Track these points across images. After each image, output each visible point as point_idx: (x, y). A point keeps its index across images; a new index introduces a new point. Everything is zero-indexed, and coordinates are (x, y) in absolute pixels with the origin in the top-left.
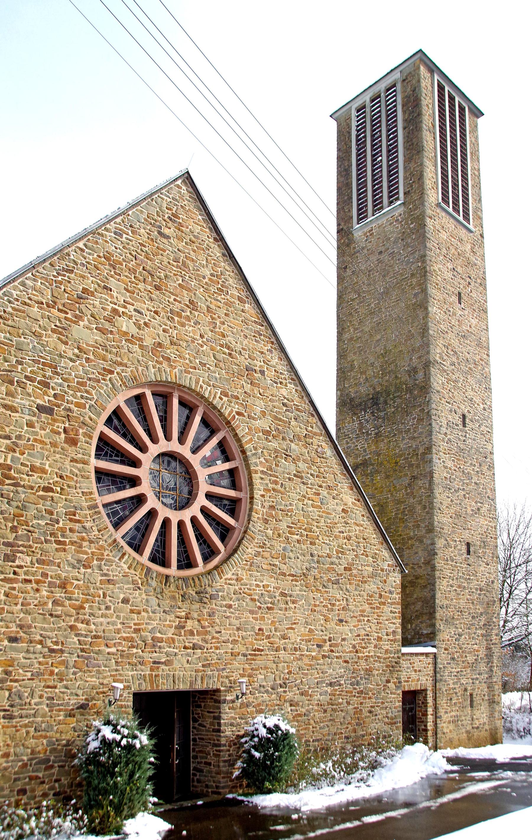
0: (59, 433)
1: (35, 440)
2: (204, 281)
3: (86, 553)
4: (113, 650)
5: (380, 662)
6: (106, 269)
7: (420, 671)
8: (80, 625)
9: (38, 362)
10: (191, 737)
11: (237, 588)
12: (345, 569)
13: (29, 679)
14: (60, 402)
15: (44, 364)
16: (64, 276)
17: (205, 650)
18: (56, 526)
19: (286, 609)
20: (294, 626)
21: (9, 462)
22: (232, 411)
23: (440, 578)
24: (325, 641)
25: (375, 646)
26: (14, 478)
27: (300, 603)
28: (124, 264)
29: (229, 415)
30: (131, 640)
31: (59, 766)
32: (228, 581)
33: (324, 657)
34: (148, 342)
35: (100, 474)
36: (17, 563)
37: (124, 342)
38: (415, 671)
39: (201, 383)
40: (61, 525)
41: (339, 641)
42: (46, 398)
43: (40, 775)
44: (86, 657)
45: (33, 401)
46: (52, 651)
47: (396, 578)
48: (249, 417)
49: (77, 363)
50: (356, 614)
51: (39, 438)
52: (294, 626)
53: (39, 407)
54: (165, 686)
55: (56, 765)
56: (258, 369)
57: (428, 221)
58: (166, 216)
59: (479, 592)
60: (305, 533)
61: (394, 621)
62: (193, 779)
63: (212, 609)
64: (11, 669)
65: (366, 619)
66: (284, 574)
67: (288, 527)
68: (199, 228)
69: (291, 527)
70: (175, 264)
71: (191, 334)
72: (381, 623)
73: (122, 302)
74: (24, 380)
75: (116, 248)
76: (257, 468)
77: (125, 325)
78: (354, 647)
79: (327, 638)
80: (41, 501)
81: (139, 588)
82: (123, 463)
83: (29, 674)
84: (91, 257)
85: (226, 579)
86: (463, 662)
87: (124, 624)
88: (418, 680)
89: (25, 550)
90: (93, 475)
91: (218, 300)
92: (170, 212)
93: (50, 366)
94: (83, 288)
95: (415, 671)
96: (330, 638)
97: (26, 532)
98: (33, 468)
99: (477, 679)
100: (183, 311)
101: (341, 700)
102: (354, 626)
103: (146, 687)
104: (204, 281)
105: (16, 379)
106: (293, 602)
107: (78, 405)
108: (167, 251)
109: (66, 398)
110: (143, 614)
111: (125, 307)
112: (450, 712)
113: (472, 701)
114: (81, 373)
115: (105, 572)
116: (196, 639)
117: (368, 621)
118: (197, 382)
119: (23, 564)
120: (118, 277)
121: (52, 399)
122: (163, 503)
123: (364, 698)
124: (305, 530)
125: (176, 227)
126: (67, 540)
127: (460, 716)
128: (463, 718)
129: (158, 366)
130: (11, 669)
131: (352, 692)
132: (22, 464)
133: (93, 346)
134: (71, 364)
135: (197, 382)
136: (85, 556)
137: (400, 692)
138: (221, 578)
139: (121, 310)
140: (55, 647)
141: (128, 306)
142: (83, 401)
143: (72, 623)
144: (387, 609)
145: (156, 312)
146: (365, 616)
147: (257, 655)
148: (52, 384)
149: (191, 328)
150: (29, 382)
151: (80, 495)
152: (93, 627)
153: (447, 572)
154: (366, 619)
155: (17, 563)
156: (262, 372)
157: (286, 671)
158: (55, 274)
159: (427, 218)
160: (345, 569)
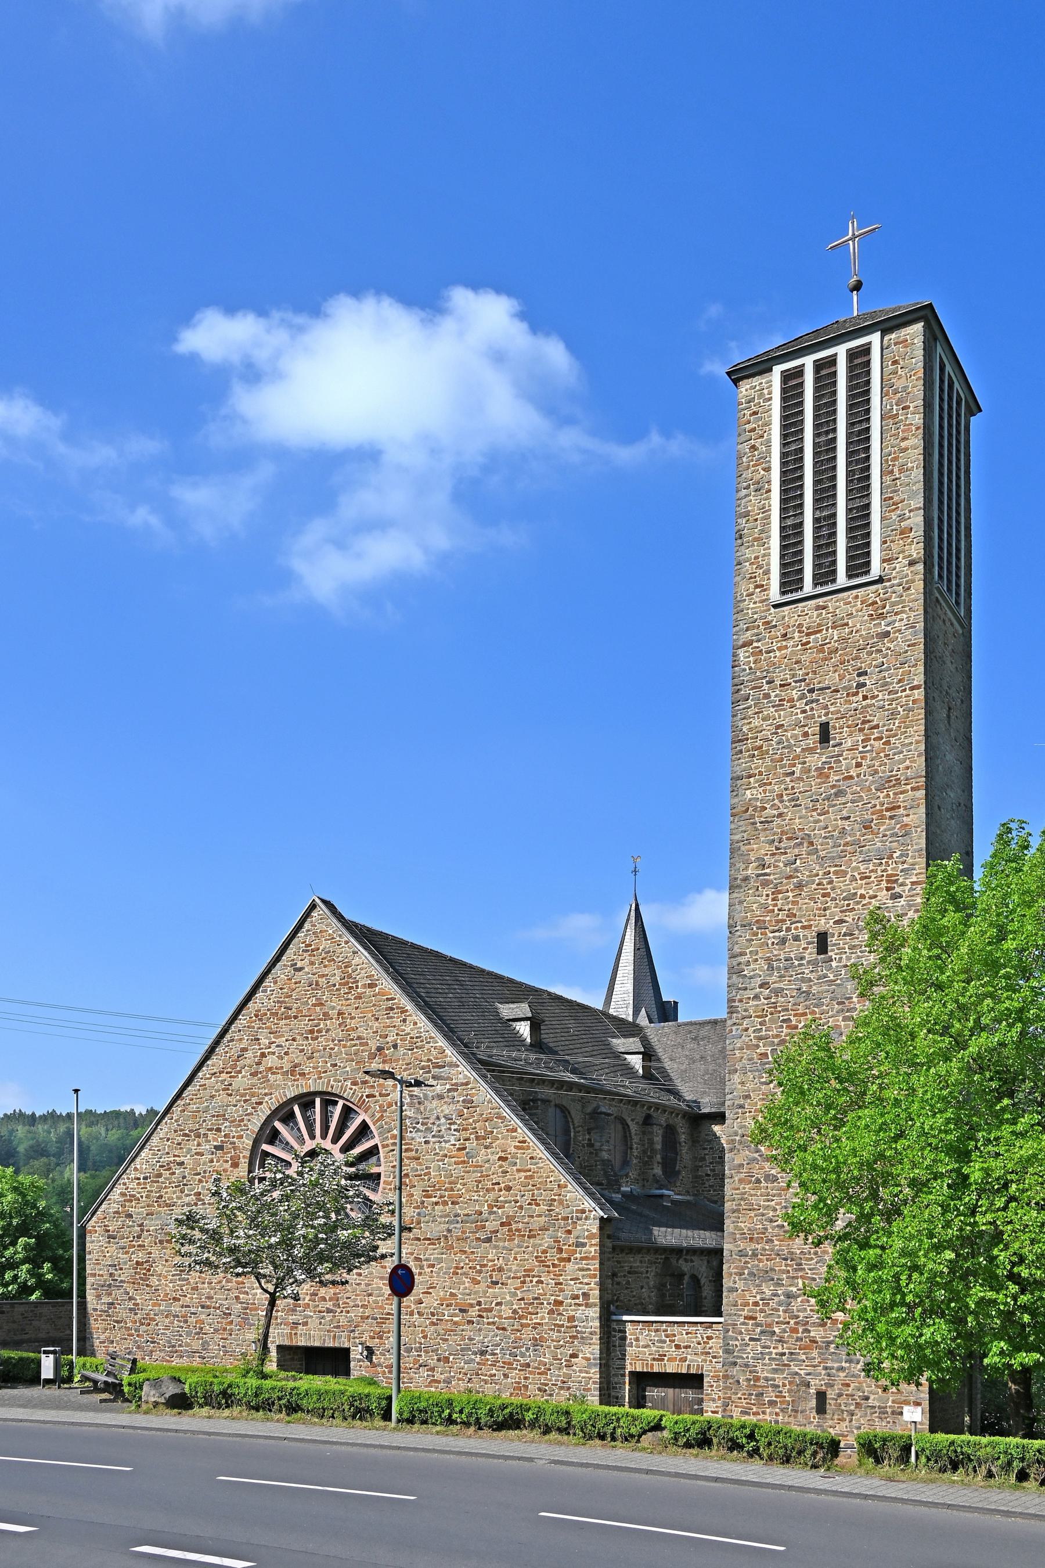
38: (678, 1347)
77: (271, 1061)
95: (678, 1347)
116: (329, 1305)
160: (502, 1224)
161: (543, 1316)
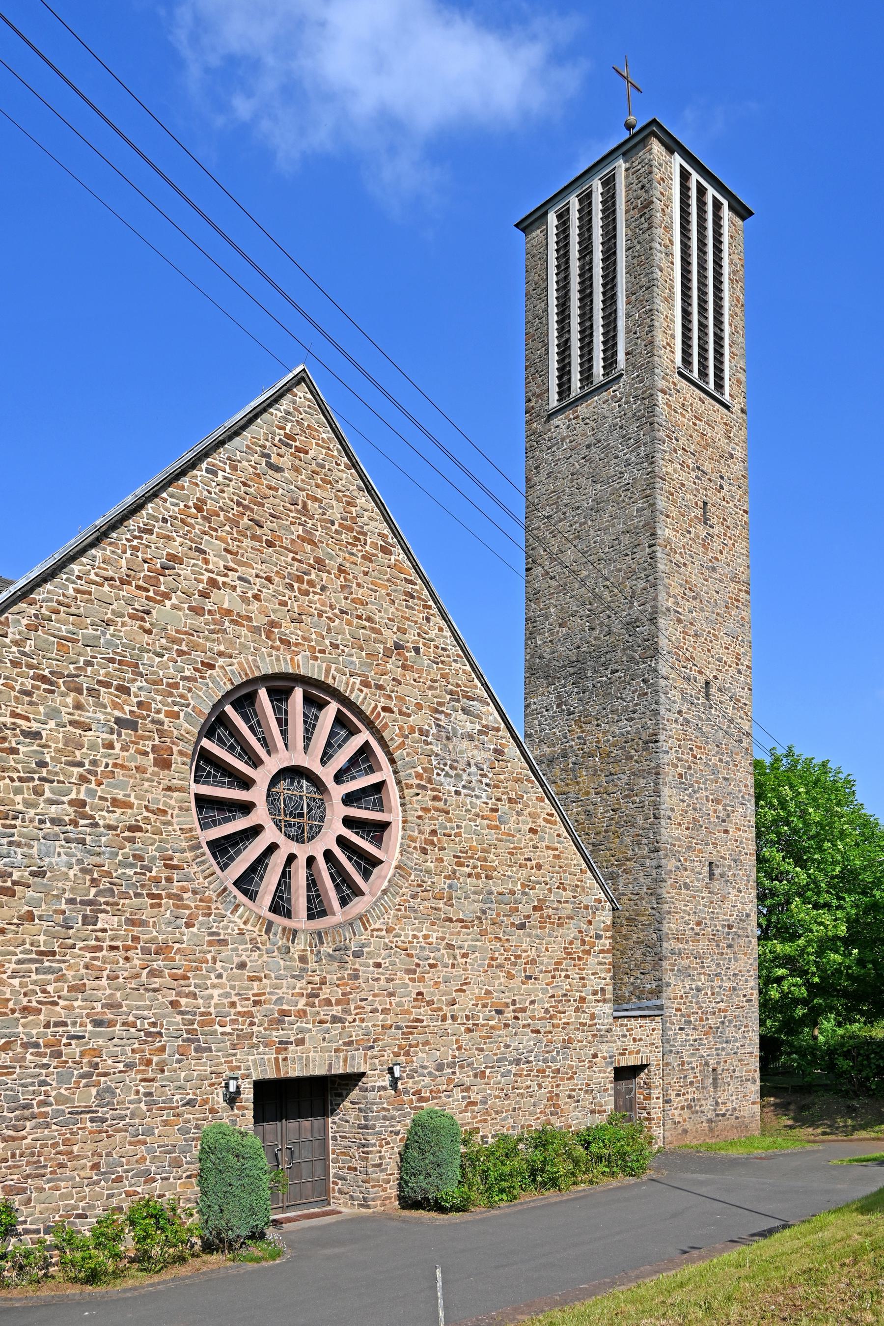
0: (146, 753)
1: (115, 765)
2: (333, 528)
3: (188, 907)
4: (228, 1029)
5: (583, 1031)
6: (199, 525)
7: (641, 1040)
8: (183, 1001)
9: (112, 660)
10: (331, 1135)
11: (387, 940)
12: (535, 908)
13: (120, 1072)
14: (145, 713)
15: (120, 663)
16: (141, 538)
17: (347, 1024)
18: (148, 874)
19: (453, 965)
20: (464, 987)
21: (82, 796)
22: (376, 707)
23: (669, 913)
24: (507, 1005)
25: (577, 1010)
26: (92, 817)
27: (473, 956)
28: (222, 514)
29: (373, 712)
30: (250, 1015)
31: (162, 1179)
32: (375, 933)
33: (506, 1025)
34: (259, 621)
35: (202, 802)
36: (100, 925)
37: (227, 624)
38: (634, 1040)
39: (333, 671)
40: (154, 874)
41: (527, 1004)
42: (127, 708)
43: (139, 1190)
44: (193, 1042)
45: (109, 714)
46: (148, 1034)
47: (605, 917)
48: (401, 713)
49: (165, 658)
50: (550, 968)
51: (119, 761)
52: (464, 987)
53: (118, 721)
54: (295, 1071)
55: (158, 1177)
56: (410, 645)
57: (660, 398)
58: (277, 439)
59: (726, 930)
60: (479, 864)
61: (603, 975)
62: (334, 1189)
63: (355, 970)
64: (97, 1060)
65: (563, 974)
66: (450, 920)
67: (455, 856)
68: (324, 451)
69: (459, 857)
70: (293, 507)
71: (318, 605)
72: (583, 978)
73: (222, 569)
74: (96, 687)
75: (210, 493)
76: (409, 782)
77: (226, 599)
78: (547, 1011)
79: (510, 1001)
80: (128, 844)
81: (258, 948)
82: (230, 785)
83: (121, 1065)
84: (176, 509)
85: (372, 930)
86: (704, 1027)
87: (240, 995)
88: (638, 1052)
89: (108, 908)
90: (193, 805)
91: (353, 554)
92: (282, 432)
93: (128, 664)
94: (168, 554)
96: (514, 1001)
97: (108, 885)
98: (115, 802)
99: (723, 1049)
100: (305, 573)
101: (529, 1083)
102: (547, 984)
103: (271, 1075)
104: (333, 528)
105: (85, 685)
106: (465, 956)
107: (169, 714)
108: (280, 491)
109: (153, 706)
110: (264, 981)
111: (226, 575)
112: (684, 1094)
113: (715, 1079)
114: (172, 671)
115: (214, 930)
116: (336, 1011)
117: (567, 977)
118: (328, 671)
119: (107, 926)
120: (214, 534)
121: (135, 709)
122: (286, 834)
123: (562, 1079)
124: (478, 859)
125: (292, 454)
126: (163, 893)
127: (699, 1100)
128: (703, 1102)
129: (274, 652)
130: (97, 1060)
131: (544, 1071)
132: (101, 798)
133: (186, 633)
134: (158, 659)
135: (328, 671)
136: (187, 912)
137: (610, 1069)
138: (366, 929)
139: (221, 579)
140: (152, 1029)
141: (230, 573)
142: (176, 709)
143: (174, 998)
144: (591, 960)
145: (269, 579)
146: (562, 970)
147: (416, 1027)
148: (132, 689)
149: (317, 597)
150: (103, 689)
151: (179, 833)
152: (200, 1001)
153: (680, 905)
154: (563, 974)
155: (100, 925)
156: (417, 650)
157: (455, 1047)
158: (129, 537)
159: (659, 393)
161: (570, 1015)
